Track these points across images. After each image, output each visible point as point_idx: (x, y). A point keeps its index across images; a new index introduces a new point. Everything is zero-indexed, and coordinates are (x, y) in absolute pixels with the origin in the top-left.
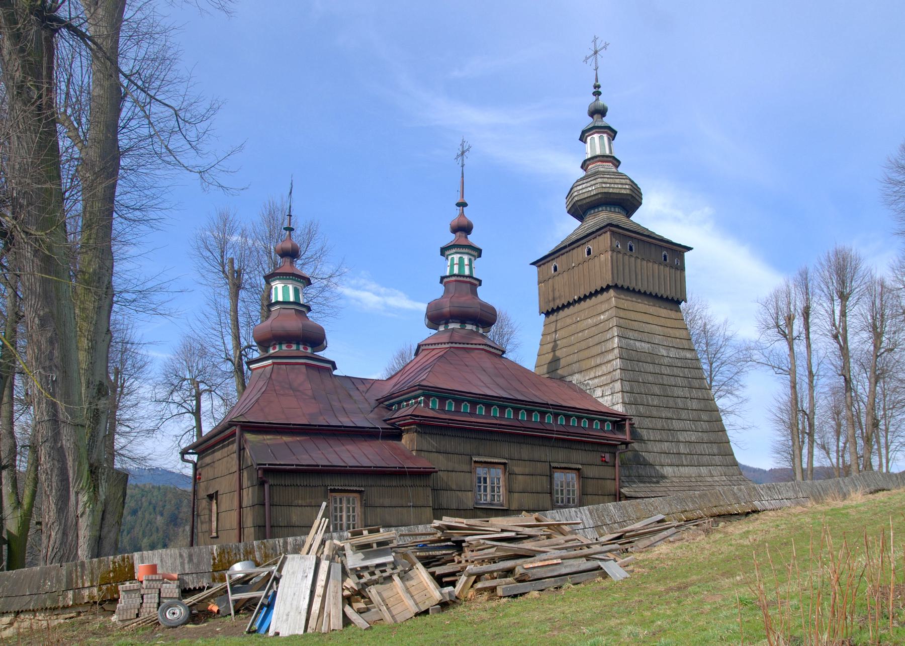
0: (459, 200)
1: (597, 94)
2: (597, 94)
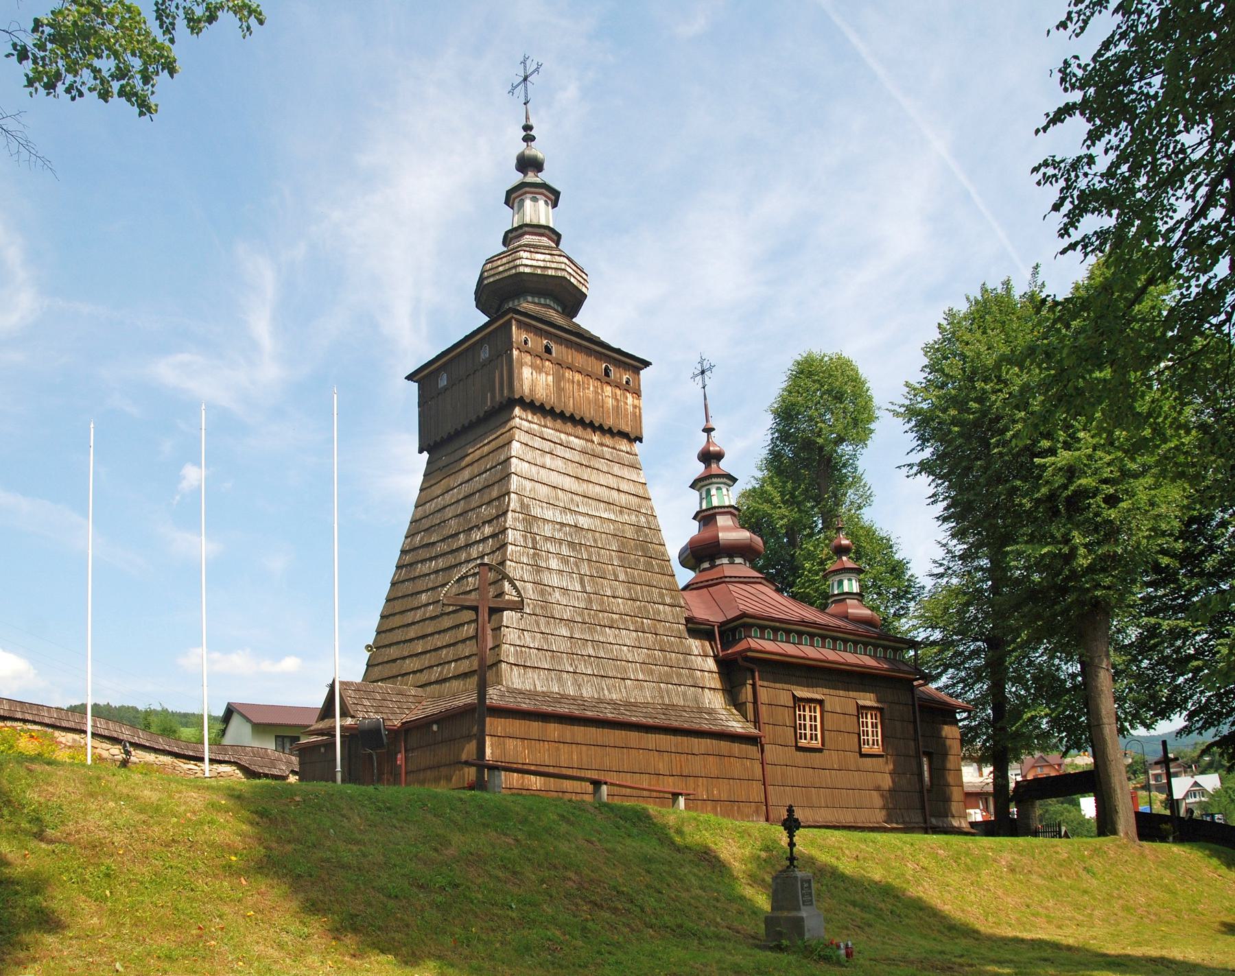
0: (703, 424)
2: (528, 139)
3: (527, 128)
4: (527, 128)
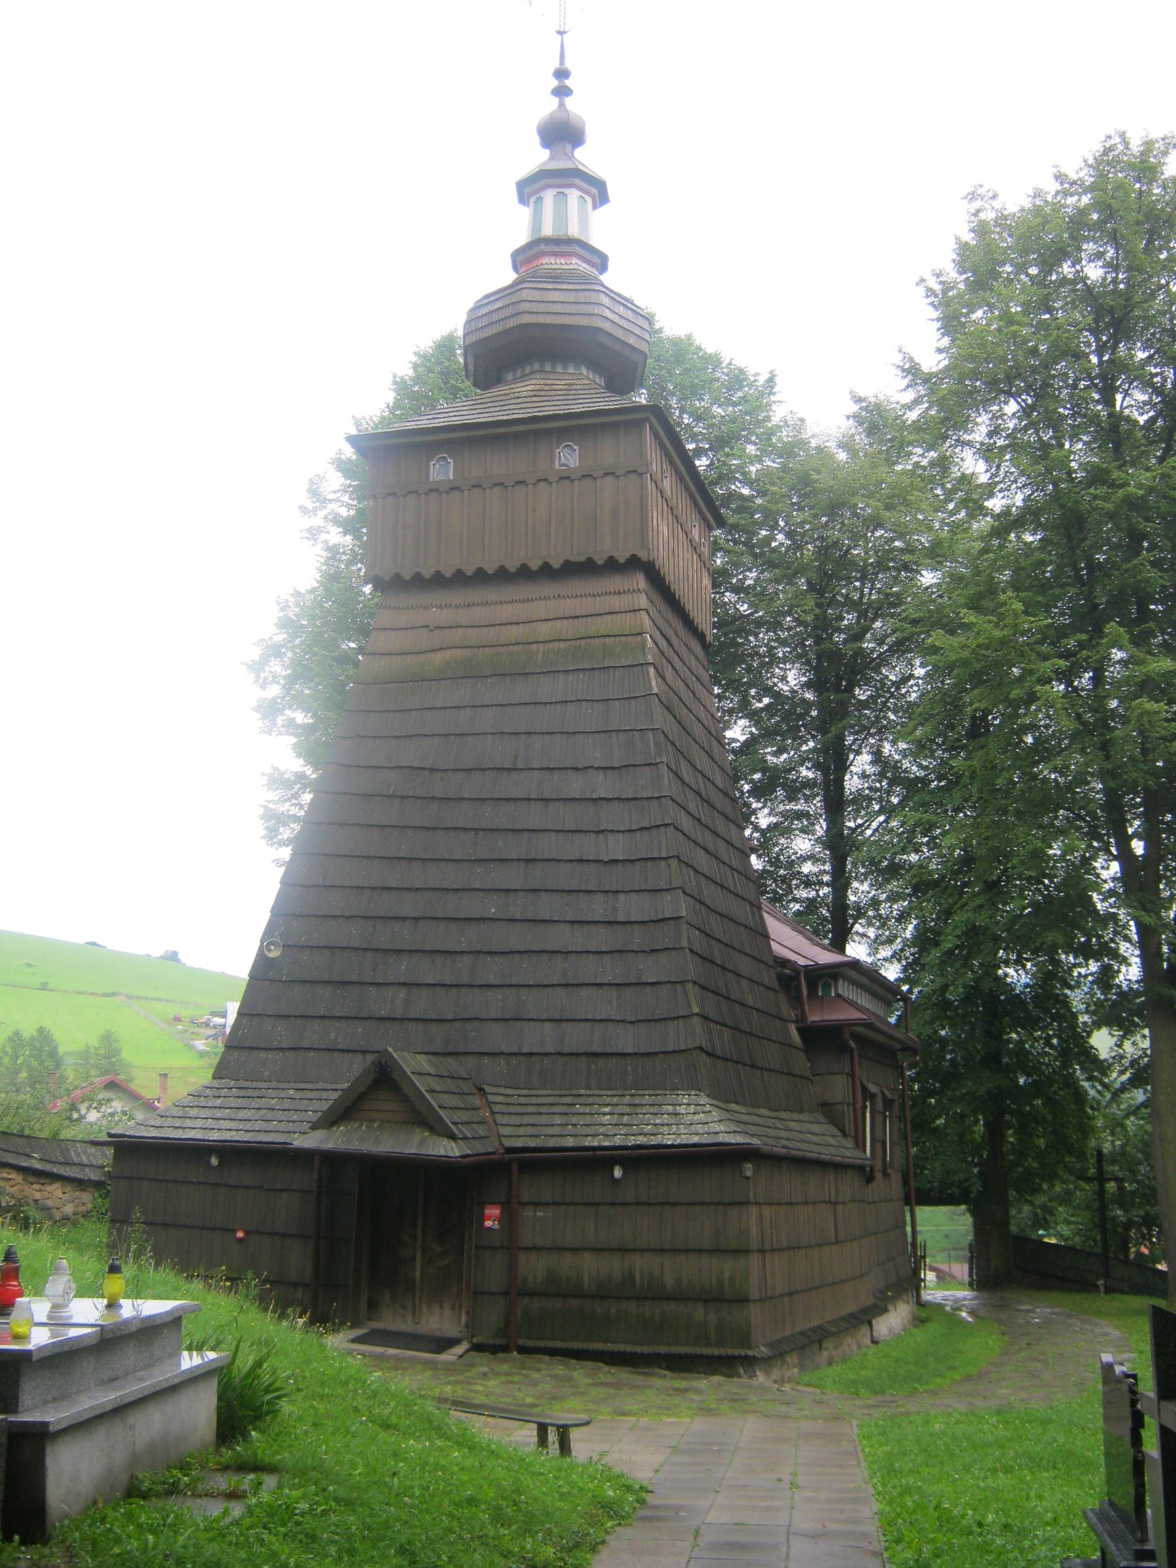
1: (562, 92)
2: (562, 92)
3: (562, 74)
4: (562, 74)
